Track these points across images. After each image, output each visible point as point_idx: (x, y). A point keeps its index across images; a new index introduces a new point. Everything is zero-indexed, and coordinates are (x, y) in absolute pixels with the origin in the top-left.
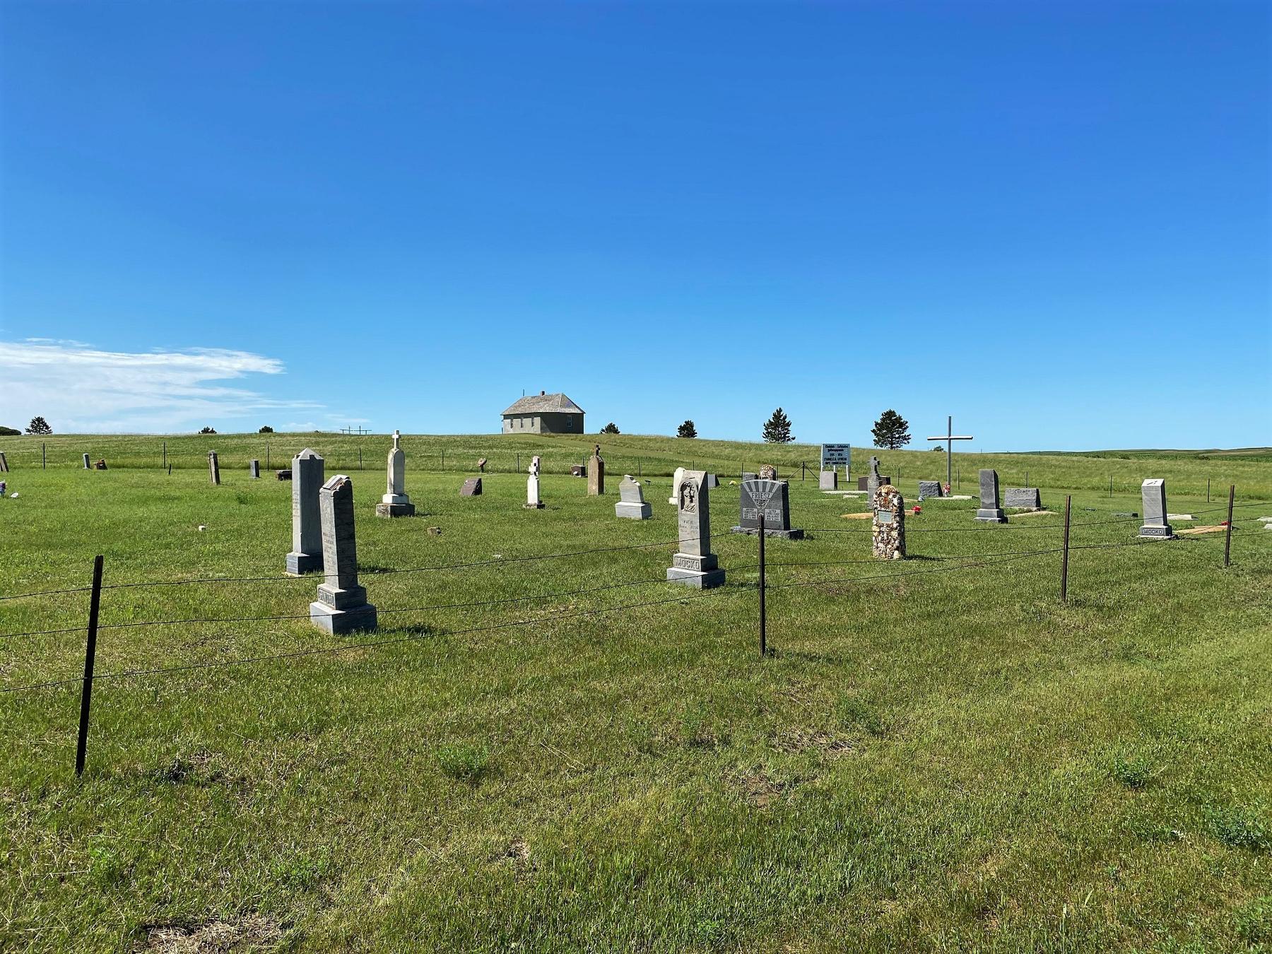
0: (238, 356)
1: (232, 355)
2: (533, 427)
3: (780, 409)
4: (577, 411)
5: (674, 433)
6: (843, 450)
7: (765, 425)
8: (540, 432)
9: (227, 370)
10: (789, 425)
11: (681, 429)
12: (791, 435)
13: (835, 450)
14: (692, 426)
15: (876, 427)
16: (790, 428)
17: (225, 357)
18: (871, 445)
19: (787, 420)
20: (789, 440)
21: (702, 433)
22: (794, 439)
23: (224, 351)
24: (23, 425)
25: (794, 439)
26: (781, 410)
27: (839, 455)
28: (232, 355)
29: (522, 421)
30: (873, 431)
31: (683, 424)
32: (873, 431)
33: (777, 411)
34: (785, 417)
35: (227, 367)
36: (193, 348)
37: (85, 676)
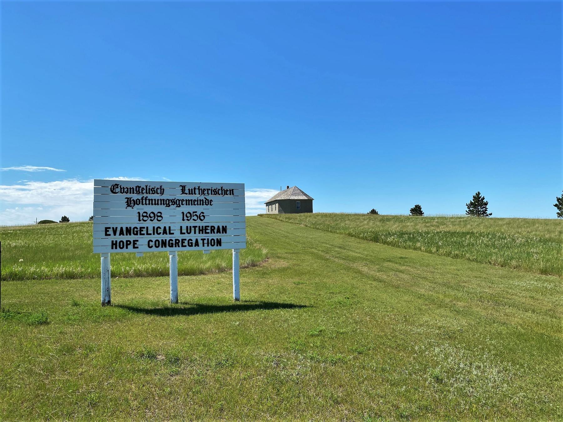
0: (271, 191)
1: (269, 191)
2: (275, 210)
3: (479, 193)
4: (304, 198)
5: (408, 213)
6: (209, 202)
7: (467, 205)
8: (278, 213)
9: (268, 197)
10: (486, 204)
11: (412, 210)
12: (488, 212)
13: (168, 203)
14: (421, 209)
15: (559, 202)
16: (487, 207)
17: (266, 192)
18: (555, 216)
19: (485, 201)
20: (487, 215)
21: (427, 211)
22: (491, 214)
23: (266, 189)
24: (58, 219)
25: (491, 214)
26: (479, 193)
27: (186, 216)
28: (269, 191)
29: (269, 207)
30: (556, 205)
31: (413, 207)
32: (556, 205)
33: (476, 194)
34: (484, 198)
35: (268, 196)
36: (27, 167)
37: (279, 308)
